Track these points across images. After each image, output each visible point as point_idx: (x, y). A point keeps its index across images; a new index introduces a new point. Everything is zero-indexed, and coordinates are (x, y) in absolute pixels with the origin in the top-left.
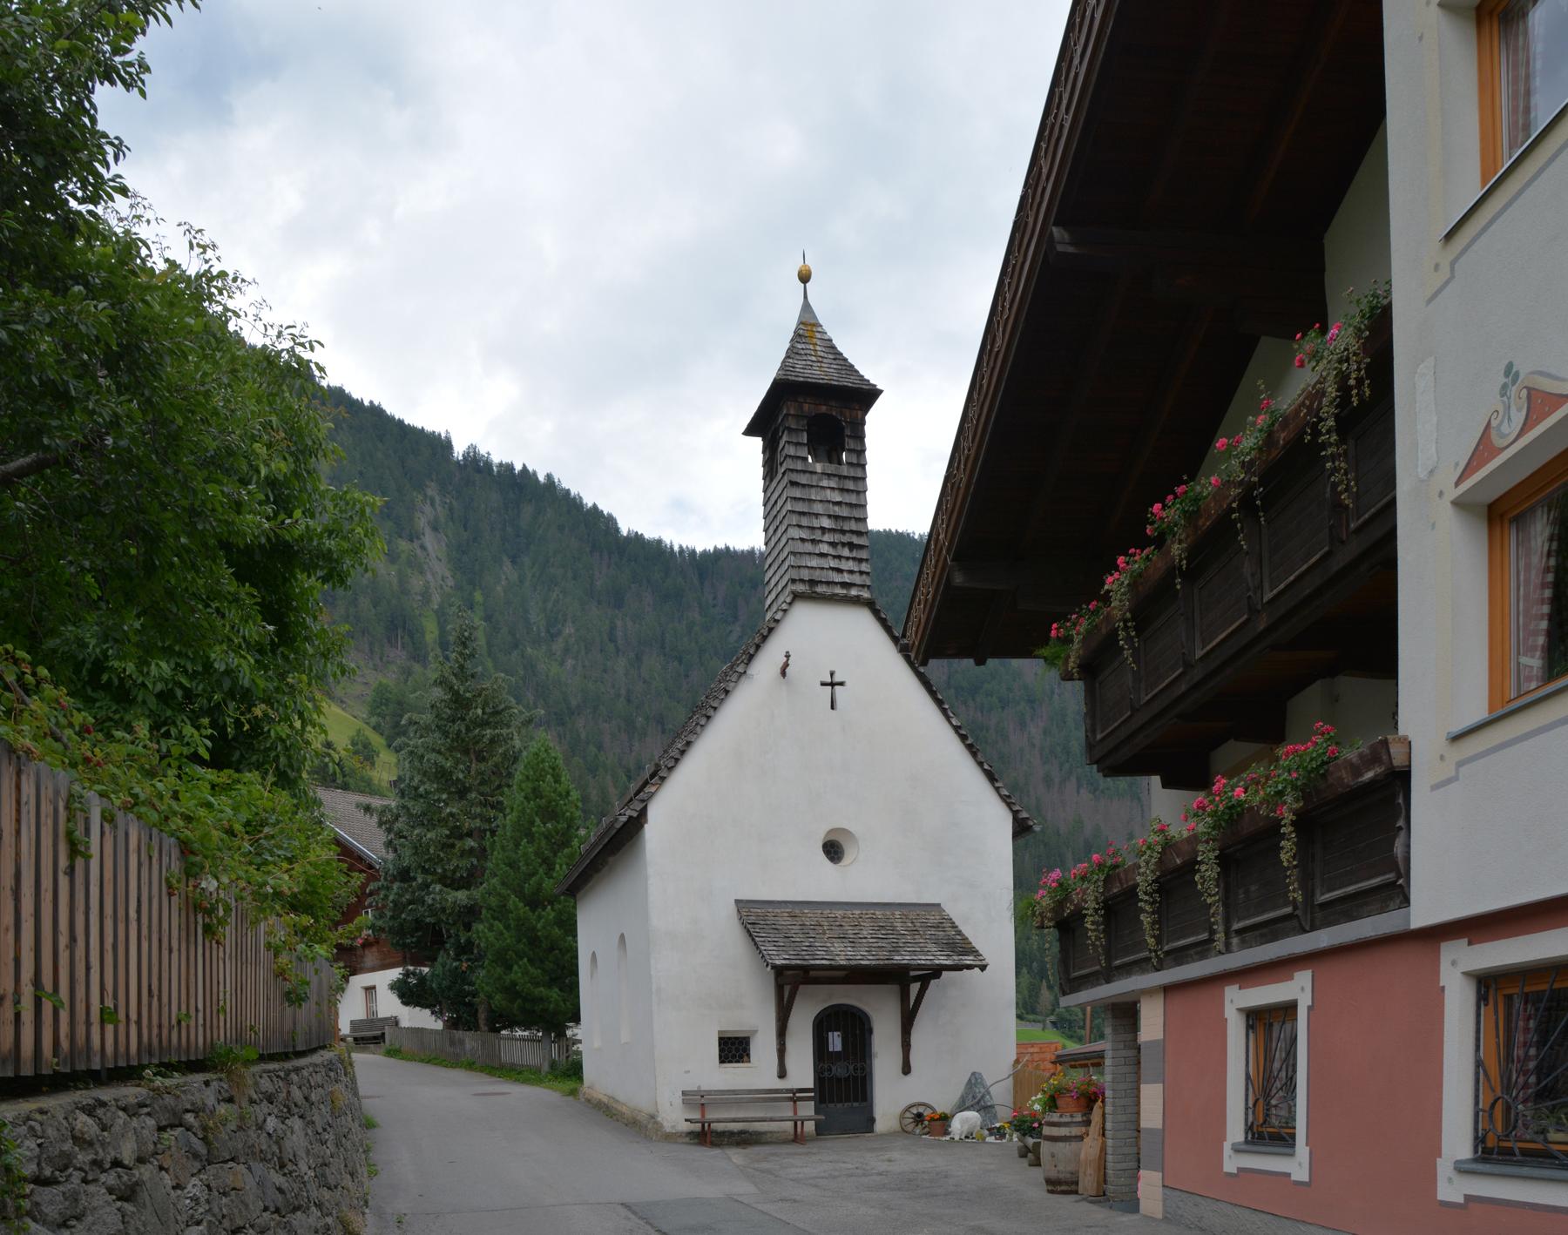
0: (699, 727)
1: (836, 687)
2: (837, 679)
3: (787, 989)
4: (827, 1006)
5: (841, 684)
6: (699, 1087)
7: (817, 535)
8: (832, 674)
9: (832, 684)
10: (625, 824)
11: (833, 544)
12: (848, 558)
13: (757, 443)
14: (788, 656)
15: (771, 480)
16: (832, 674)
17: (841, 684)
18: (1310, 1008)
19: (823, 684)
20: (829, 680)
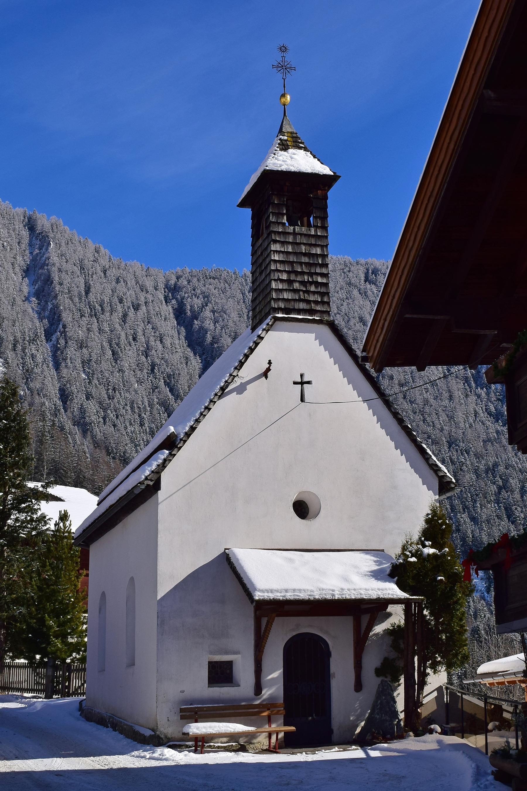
0: (202, 416)
1: (305, 385)
2: (306, 379)
3: (264, 621)
4: (294, 634)
5: (309, 383)
6: (475, 714)
7: (293, 277)
8: (302, 376)
9: (302, 383)
10: (143, 490)
11: (302, 283)
12: (314, 293)
13: (248, 212)
14: (270, 363)
15: (258, 239)
16: (302, 376)
17: (309, 383)
18: (431, 456)
19: (295, 383)
20: (299, 380)
